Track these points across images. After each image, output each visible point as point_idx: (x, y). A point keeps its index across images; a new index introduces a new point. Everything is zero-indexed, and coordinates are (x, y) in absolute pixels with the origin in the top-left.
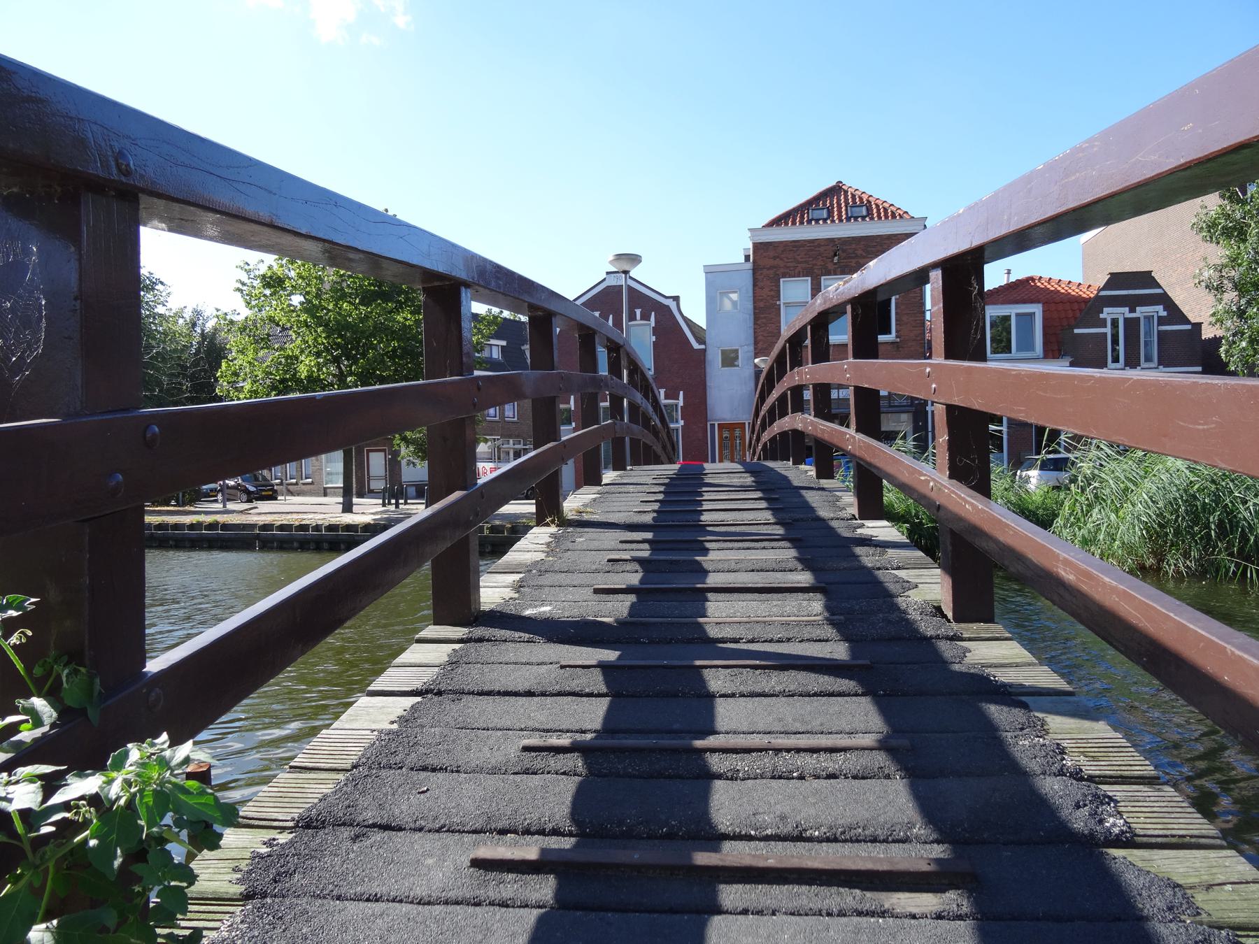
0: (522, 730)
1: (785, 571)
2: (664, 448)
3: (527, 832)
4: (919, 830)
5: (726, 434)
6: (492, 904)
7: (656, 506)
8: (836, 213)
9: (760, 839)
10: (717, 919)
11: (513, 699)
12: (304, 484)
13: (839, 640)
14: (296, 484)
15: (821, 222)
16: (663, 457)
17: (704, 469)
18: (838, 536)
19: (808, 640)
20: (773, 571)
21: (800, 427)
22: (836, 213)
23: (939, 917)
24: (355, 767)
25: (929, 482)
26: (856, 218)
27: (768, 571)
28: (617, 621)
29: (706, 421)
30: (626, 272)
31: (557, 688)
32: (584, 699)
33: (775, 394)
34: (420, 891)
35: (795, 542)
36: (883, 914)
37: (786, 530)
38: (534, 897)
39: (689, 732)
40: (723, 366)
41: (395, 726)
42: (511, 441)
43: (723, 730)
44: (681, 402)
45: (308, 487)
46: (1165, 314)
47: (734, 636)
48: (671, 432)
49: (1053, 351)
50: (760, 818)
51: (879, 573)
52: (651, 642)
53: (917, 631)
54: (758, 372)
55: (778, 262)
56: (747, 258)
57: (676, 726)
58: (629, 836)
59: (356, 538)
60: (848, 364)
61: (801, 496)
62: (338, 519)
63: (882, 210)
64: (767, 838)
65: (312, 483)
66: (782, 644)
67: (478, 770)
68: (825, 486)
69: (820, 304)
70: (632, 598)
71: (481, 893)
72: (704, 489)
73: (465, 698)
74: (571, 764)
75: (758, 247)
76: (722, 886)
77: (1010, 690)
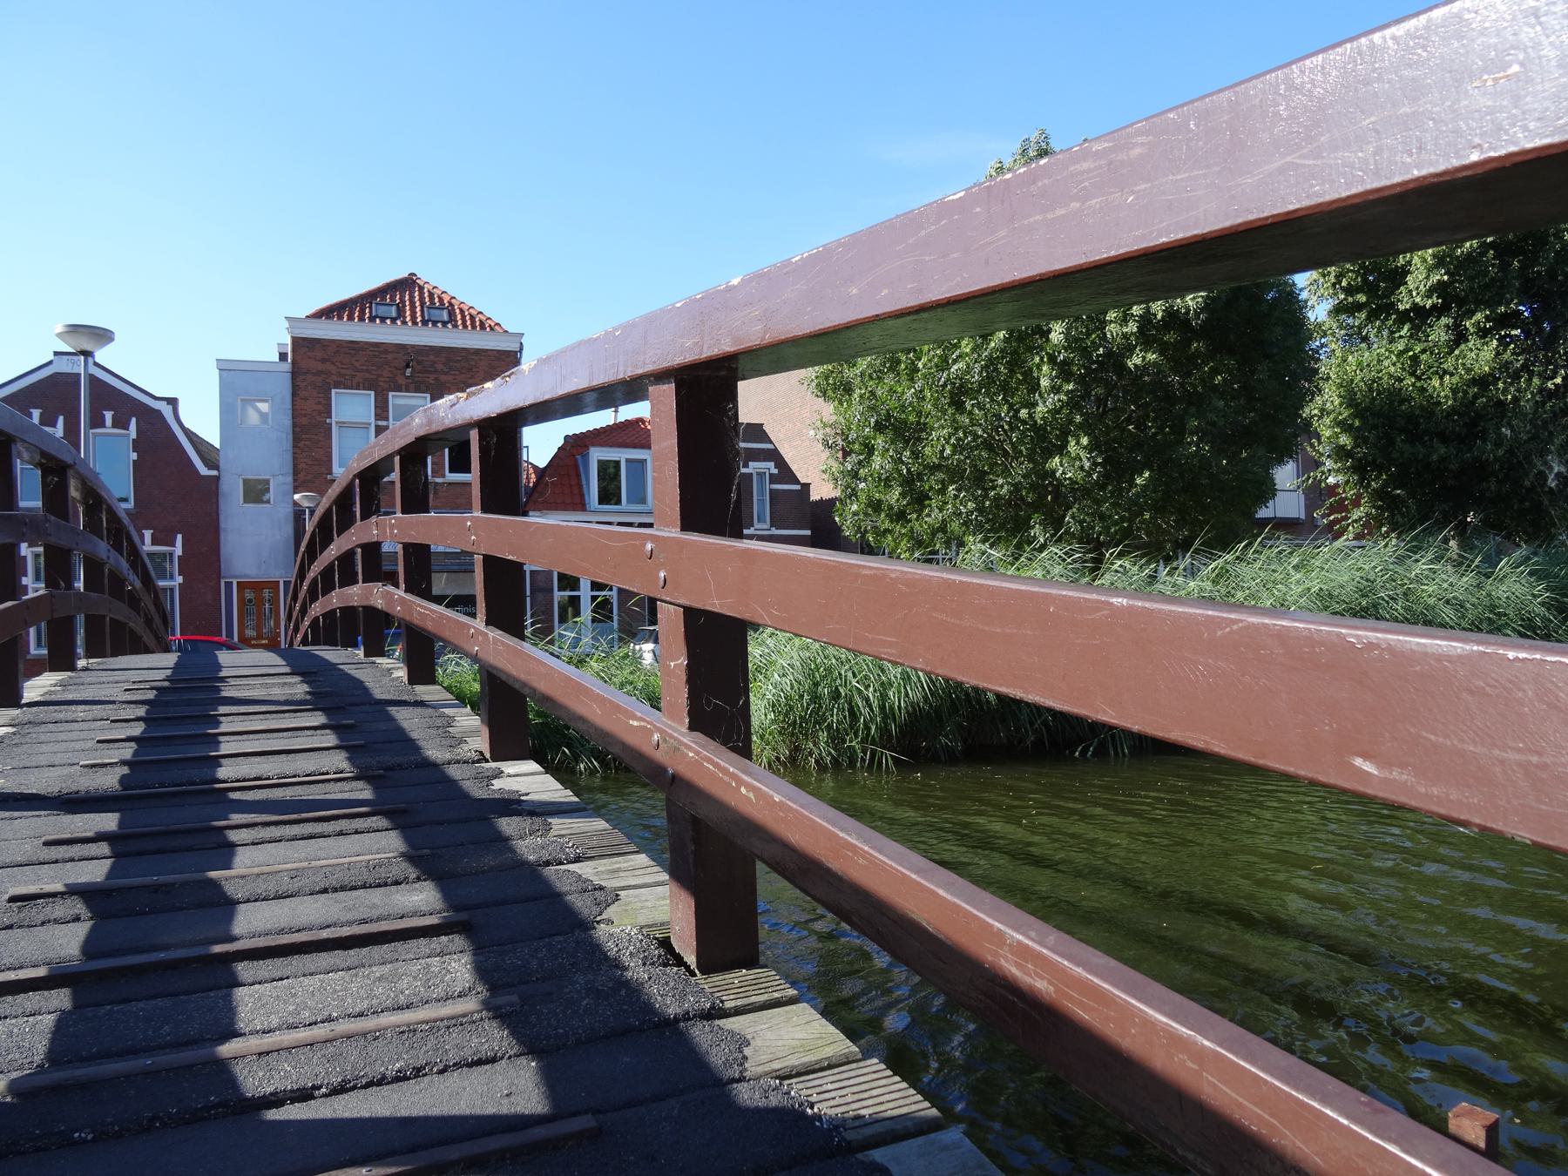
1: (386, 885)
2: (149, 622)
5: (249, 595)
7: (127, 752)
8: (408, 313)
13: (517, 1056)
15: (388, 321)
16: (148, 638)
17: (219, 667)
18: (465, 796)
19: (458, 1065)
20: (364, 887)
21: (379, 603)
22: (408, 313)
25: (651, 733)
26: (435, 323)
29: (219, 577)
30: (87, 354)
33: (333, 551)
35: (399, 817)
37: (376, 789)
40: (245, 501)
44: (178, 550)
46: (775, 471)
47: (301, 1084)
48: (161, 596)
51: (550, 871)
53: (648, 1008)
54: (298, 515)
55: (328, 366)
56: (283, 356)
60: (473, 519)
61: (391, 719)
63: (468, 318)
66: (404, 1085)
68: (426, 698)
69: (421, 426)
70: (61, 999)
72: (223, 709)
75: (297, 342)
77: (850, 1135)
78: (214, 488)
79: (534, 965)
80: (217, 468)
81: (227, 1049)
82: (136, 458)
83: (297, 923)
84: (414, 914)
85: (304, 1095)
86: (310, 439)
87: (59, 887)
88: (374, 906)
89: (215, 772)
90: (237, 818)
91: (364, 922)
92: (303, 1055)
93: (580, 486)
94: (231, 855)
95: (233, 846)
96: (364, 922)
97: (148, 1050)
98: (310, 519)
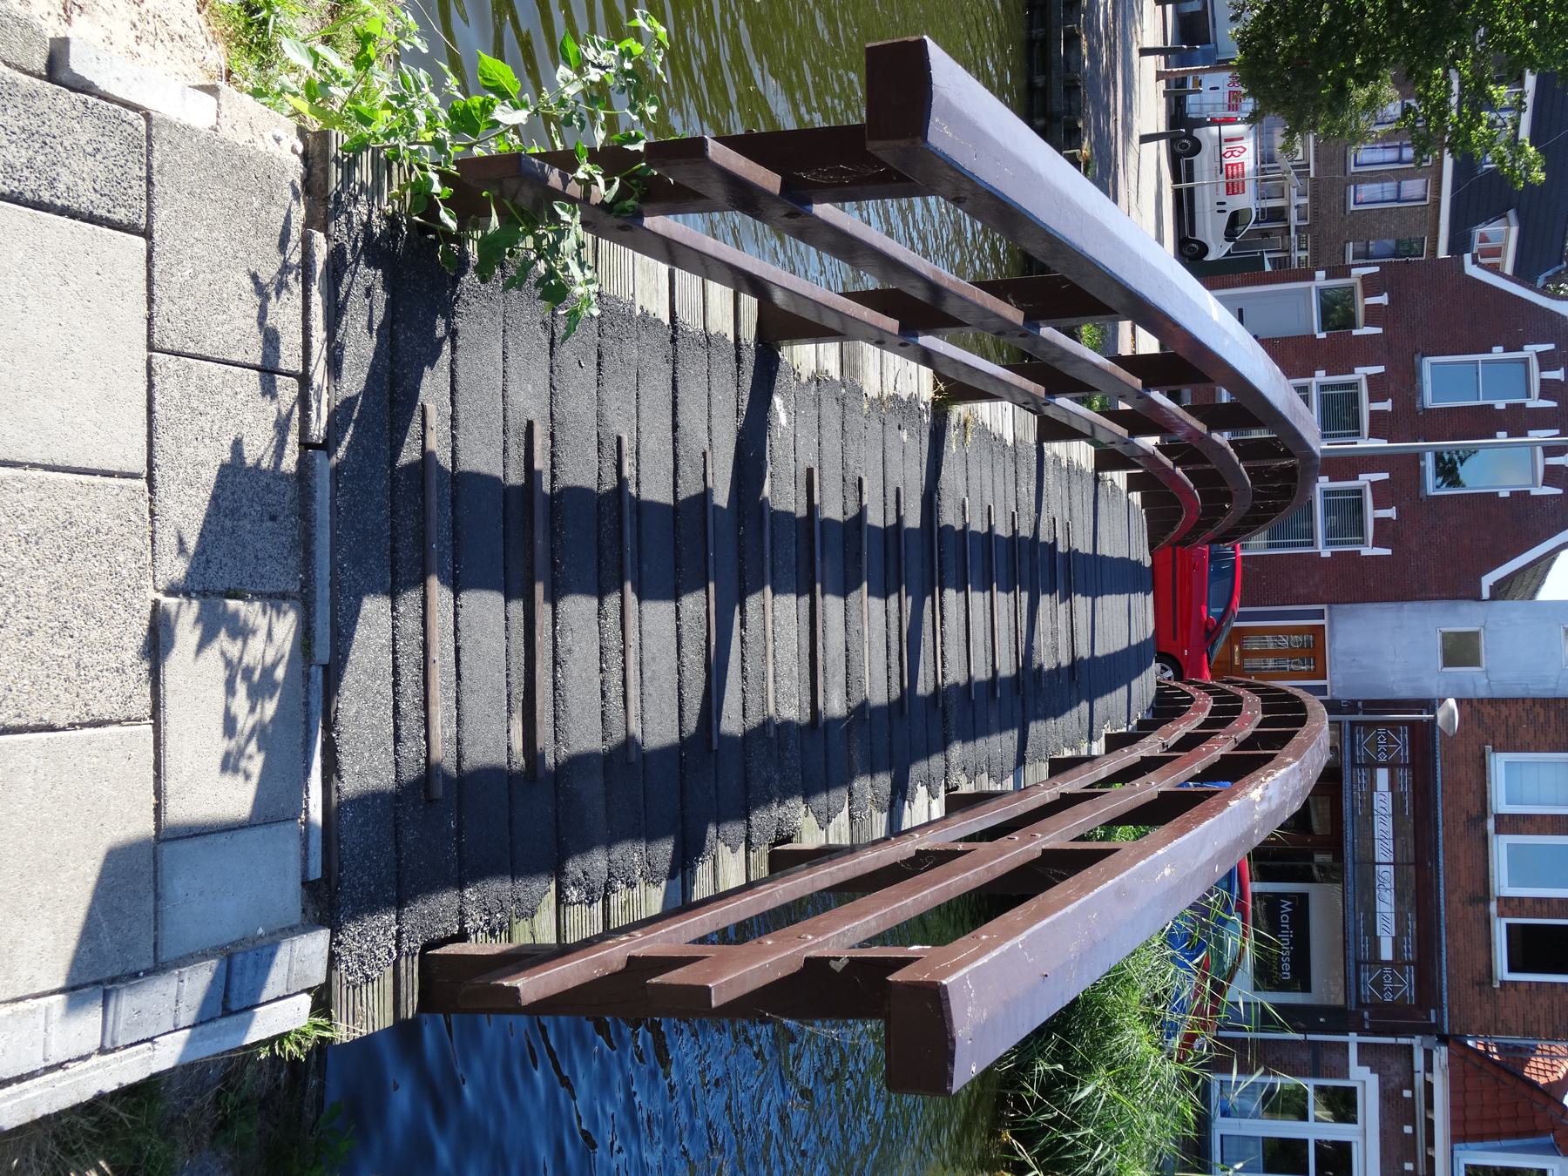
0: (638, 429)
3: (553, 455)
4: (564, 752)
6: (505, 442)
11: (669, 412)
23: (509, 748)
27: (847, 667)
28: (766, 499)
31: (682, 453)
32: (671, 480)
34: (511, 389)
36: (509, 711)
38: (510, 472)
40: (1445, 636)
41: (638, 312)
42: (1305, 201)
44: (1368, 551)
52: (740, 538)
54: (1429, 705)
57: (645, 567)
58: (553, 534)
64: (554, 638)
72: (1025, 596)
74: (608, 479)
79: (788, 755)
80: (1493, 598)
81: (768, 589)
82: (1501, 495)
83: (828, 631)
84: (826, 699)
85: (743, 624)
86: (1548, 721)
87: (865, 502)
89: (951, 587)
90: (908, 602)
92: (760, 625)
93: (1498, 1136)
94: (878, 595)
95: (886, 598)
97: (772, 555)
98: (1304, 688)
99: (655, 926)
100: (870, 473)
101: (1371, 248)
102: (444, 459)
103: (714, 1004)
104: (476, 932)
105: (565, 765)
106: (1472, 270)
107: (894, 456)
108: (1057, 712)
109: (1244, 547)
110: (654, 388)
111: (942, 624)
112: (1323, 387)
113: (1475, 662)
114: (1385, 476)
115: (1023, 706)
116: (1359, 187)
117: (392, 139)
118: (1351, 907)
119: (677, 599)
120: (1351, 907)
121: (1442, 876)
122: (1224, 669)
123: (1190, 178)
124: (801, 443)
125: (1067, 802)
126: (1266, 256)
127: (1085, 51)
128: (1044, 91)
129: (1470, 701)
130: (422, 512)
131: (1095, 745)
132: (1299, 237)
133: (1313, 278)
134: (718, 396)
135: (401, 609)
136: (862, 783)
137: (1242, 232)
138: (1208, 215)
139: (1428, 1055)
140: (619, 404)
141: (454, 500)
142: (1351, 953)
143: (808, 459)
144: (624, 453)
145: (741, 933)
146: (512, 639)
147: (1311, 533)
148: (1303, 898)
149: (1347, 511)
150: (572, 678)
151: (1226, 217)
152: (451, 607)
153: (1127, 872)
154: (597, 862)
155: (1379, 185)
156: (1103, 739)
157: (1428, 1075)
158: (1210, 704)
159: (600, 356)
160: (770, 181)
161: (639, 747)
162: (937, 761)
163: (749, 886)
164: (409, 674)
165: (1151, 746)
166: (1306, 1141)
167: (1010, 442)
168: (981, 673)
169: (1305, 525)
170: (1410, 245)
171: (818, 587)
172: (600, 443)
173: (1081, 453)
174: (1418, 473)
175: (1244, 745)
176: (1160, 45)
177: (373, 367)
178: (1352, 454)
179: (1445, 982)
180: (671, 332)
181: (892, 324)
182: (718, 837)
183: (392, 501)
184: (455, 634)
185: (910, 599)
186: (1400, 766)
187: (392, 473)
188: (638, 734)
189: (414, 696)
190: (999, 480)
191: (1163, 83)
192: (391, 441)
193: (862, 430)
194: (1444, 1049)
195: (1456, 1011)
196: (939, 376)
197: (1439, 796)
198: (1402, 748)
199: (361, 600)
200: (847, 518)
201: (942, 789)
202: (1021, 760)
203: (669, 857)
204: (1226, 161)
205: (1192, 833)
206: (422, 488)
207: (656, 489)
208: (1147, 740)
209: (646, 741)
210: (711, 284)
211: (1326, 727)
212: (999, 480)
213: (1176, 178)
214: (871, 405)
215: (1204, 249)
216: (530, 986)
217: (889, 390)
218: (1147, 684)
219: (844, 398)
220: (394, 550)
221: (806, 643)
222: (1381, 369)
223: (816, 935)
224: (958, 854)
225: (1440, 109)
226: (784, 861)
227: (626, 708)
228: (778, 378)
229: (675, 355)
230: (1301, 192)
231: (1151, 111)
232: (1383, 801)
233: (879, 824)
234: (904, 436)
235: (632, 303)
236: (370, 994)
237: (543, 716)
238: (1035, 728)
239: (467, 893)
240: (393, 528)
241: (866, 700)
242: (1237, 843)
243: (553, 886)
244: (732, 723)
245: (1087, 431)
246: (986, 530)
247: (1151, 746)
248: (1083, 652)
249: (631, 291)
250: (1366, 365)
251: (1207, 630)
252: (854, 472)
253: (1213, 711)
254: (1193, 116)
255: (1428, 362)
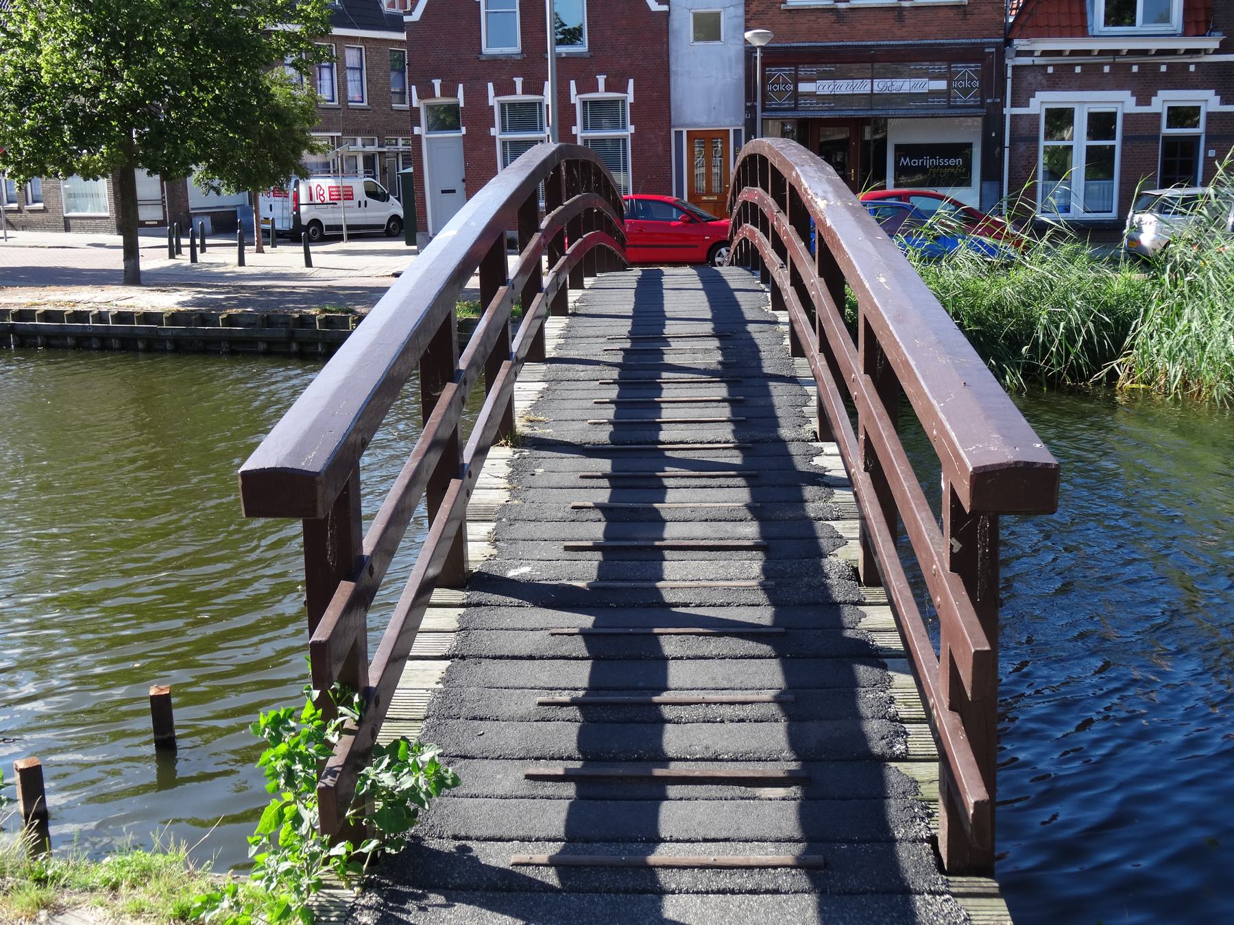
0: (532, 688)
3: (552, 758)
4: (786, 754)
6: (542, 798)
9: (692, 761)
10: (665, 803)
11: (520, 662)
12: (31, 211)
14: (19, 211)
23: (784, 799)
24: (426, 718)
27: (720, 521)
28: (589, 585)
29: (670, 127)
31: (551, 653)
32: (572, 662)
34: (500, 792)
36: (754, 799)
37: (745, 458)
38: (565, 794)
39: (649, 689)
40: (696, 39)
41: (440, 686)
42: (359, 140)
43: (673, 687)
44: (630, 97)
45: (39, 216)
49: (1197, 22)
50: (693, 748)
52: (619, 606)
54: (750, 51)
57: (641, 684)
58: (615, 760)
59: (162, 333)
62: (129, 302)
64: (697, 760)
65: (45, 210)
67: (511, 719)
71: (534, 792)
72: (665, 375)
73: (484, 662)
74: (572, 714)
76: (301, 521)
78: (660, 149)
79: (789, 570)
81: (659, 584)
85: (686, 605)
87: (591, 504)
88: (727, 532)
89: (658, 435)
90: (670, 470)
91: (721, 539)
92: (687, 591)
94: (665, 493)
95: (666, 488)
96: (721, 539)
97: (631, 580)
99: (925, 687)
100: (568, 499)
101: (398, 90)
102: (554, 848)
103: (987, 648)
104: (930, 829)
105: (797, 753)
106: (416, 16)
107: (555, 479)
108: (755, 350)
109: (626, 192)
110: (500, 674)
111: (687, 443)
112: (504, 130)
113: (717, 16)
114: (573, 83)
115: (750, 377)
116: (350, 99)
117: (302, 889)
118: (906, 112)
119: (666, 659)
120: (906, 112)
121: (882, 43)
122: (721, 207)
123: (339, 228)
124: (544, 555)
125: (825, 348)
126: (401, 171)
127: (240, 310)
128: (270, 342)
129: (747, 21)
130: (597, 867)
131: (780, 320)
132: (387, 145)
133: (419, 136)
134: (508, 623)
135: (673, 886)
136: (812, 509)
137: (382, 188)
138: (368, 214)
139: (1020, 54)
140: (512, 704)
141: (587, 841)
142: (942, 112)
143: (556, 550)
144: (551, 700)
145: (932, 620)
146: (697, 795)
147: (616, 141)
148: (899, 148)
149: (599, 112)
150: (728, 747)
151: (370, 200)
152: (672, 845)
153: (883, 313)
154: (874, 727)
155: (349, 83)
156: (776, 313)
157: (1036, 54)
158: (749, 226)
159: (475, 718)
160: (345, 590)
161: (783, 693)
162: (794, 448)
163: (891, 603)
164: (725, 881)
165: (782, 277)
166: (1088, 147)
167: (545, 385)
168: (725, 412)
169: (609, 144)
170: (396, 60)
171: (657, 543)
172: (543, 720)
173: (554, 326)
174: (570, 58)
175: (782, 206)
176: (236, 249)
177: (481, 905)
178: (556, 107)
179: (964, 41)
180: (456, 660)
181: (454, 485)
182: (854, 628)
183: (588, 892)
184: (693, 842)
185: (667, 469)
186: (796, 74)
187: (565, 891)
188: (773, 692)
189: (742, 877)
190: (575, 394)
191: (266, 248)
192: (540, 891)
193: (534, 506)
194: (1016, 42)
195: (986, 33)
196: (495, 442)
197: (820, 44)
198: (783, 72)
199: (666, 920)
200: (603, 519)
201: (816, 444)
202: (793, 380)
203: (870, 669)
204: (327, 200)
205: (852, 259)
206: (578, 867)
207: (580, 674)
208: (777, 280)
209: (778, 686)
210: (422, 627)
211: (764, 140)
212: (575, 394)
213: (339, 238)
214: (515, 498)
215: (395, 218)
216: (973, 793)
217: (503, 483)
218: (735, 276)
219: (510, 520)
220: (626, 891)
221: (701, 554)
222: (490, 86)
223: (933, 562)
224: (867, 440)
225: (291, 38)
226: (872, 575)
227: (752, 703)
228: (494, 573)
229: (475, 657)
230: (352, 142)
231: (287, 258)
232: (824, 87)
233: (843, 496)
234: (539, 471)
235: (434, 690)
236: (979, 918)
237: (758, 771)
238: (768, 368)
239: (898, 836)
240: (609, 892)
241: (746, 505)
242: (859, 220)
243: (893, 764)
244: (763, 616)
245: (538, 322)
246: (613, 406)
247: (782, 277)
248: (708, 328)
249: (424, 691)
250: (487, 97)
251: (690, 222)
252: (566, 512)
253: (755, 224)
254: (292, 224)
255: (486, 50)
